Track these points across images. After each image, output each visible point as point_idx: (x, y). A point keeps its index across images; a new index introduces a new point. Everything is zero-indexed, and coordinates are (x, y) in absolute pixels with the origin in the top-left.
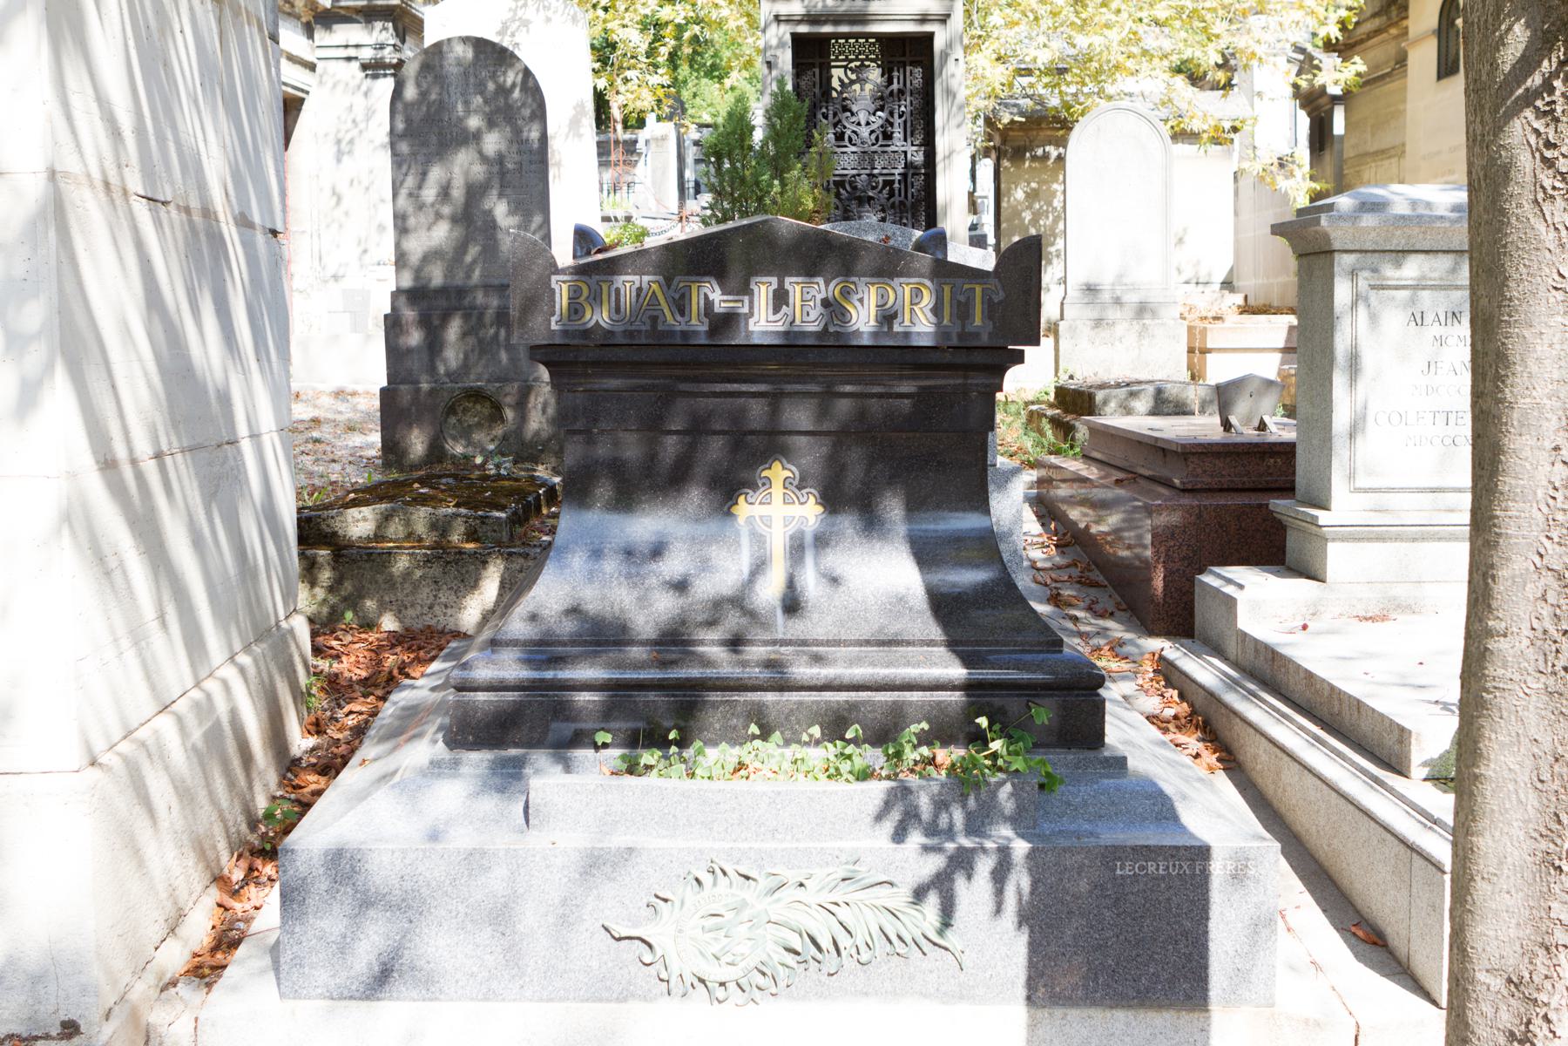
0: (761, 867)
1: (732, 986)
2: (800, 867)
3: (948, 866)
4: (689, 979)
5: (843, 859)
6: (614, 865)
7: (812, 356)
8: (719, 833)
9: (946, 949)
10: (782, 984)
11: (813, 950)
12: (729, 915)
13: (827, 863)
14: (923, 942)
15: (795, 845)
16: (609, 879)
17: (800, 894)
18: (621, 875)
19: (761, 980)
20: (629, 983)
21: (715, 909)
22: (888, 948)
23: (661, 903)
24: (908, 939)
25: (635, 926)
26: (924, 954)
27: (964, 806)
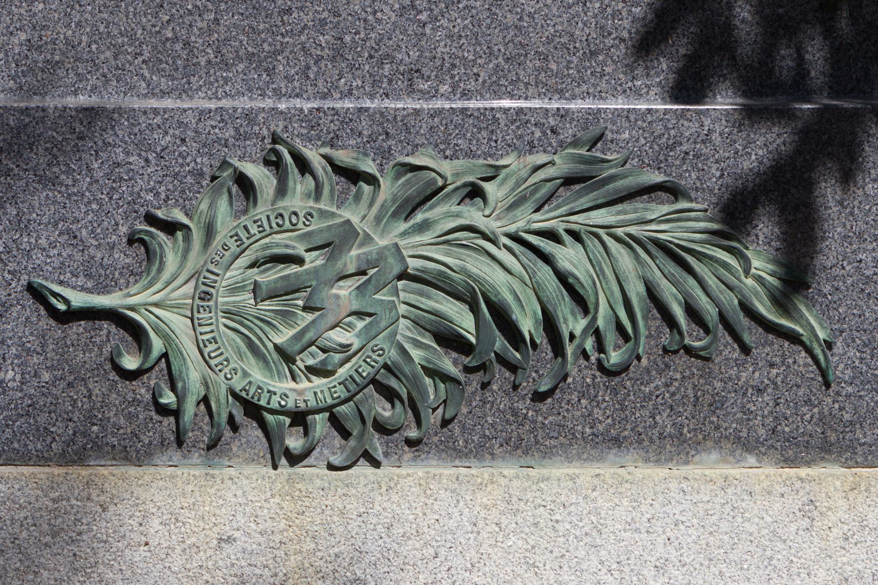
0: (384, 155)
1: (320, 422)
2: (470, 154)
3: (798, 152)
4: (224, 406)
5: (568, 132)
6: (55, 150)
7: (739, 297)
8: (288, 78)
9: (794, 338)
10: (433, 419)
11: (500, 343)
12: (314, 260)
13: (531, 145)
14: (743, 321)
15: (458, 105)
16: (42, 180)
17: (473, 215)
18: (69, 172)
19: (384, 410)
20: (90, 419)
21: (282, 242)
22: (666, 338)
23: (162, 236)
24: (710, 311)
25: (103, 289)
26: (746, 350)
27: (828, 33)
